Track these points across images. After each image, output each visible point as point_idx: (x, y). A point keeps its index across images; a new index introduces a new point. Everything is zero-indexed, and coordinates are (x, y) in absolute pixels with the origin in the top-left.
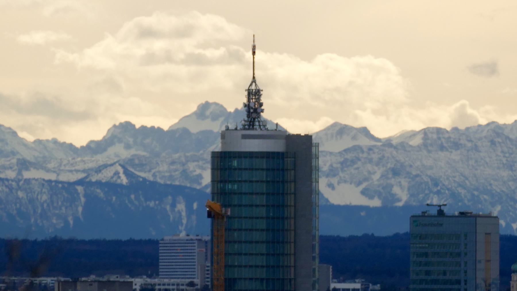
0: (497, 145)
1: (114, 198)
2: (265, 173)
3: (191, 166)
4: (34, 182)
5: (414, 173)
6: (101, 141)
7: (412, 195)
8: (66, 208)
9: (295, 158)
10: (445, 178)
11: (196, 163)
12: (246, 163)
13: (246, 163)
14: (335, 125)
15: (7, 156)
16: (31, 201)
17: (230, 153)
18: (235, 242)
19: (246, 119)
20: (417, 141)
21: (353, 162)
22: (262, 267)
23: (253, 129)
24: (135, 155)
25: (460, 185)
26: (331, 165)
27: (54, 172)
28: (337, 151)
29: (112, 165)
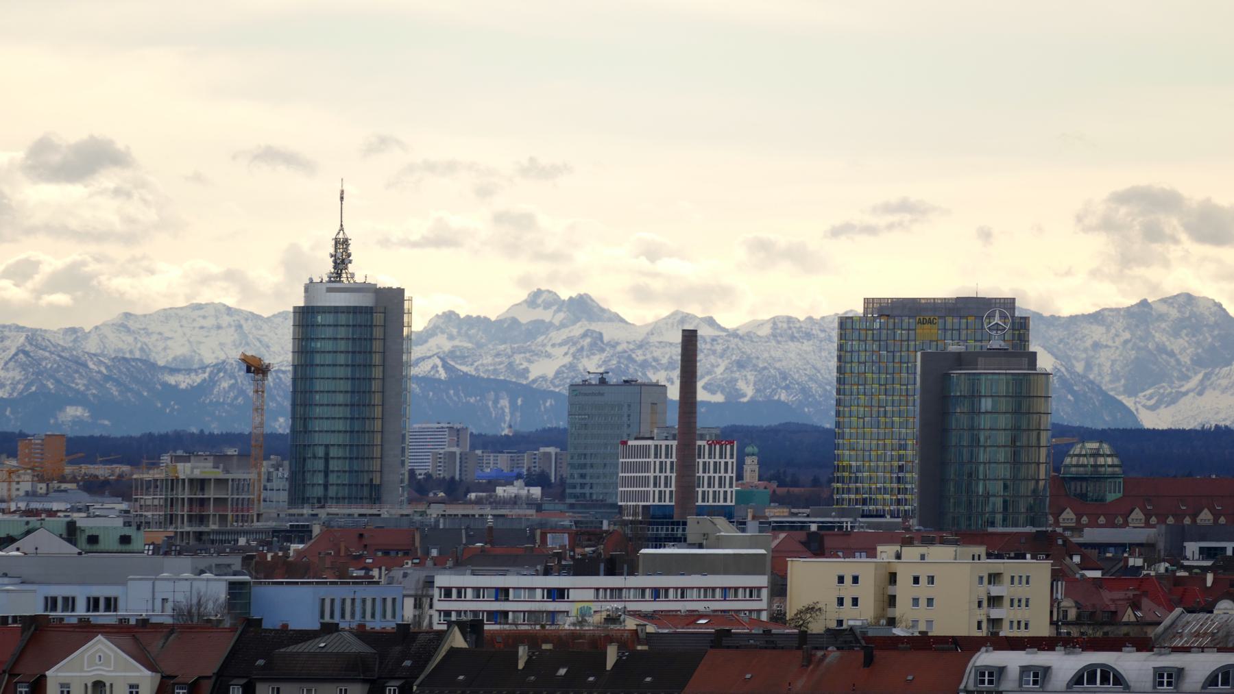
1: (431, 394)
3: (518, 358)
5: (761, 366)
6: (422, 332)
7: (758, 391)
9: (385, 313)
10: (795, 370)
11: (523, 355)
12: (330, 319)
13: (330, 319)
17: (313, 307)
19: (333, 270)
20: (765, 331)
23: (340, 281)
24: (457, 346)
25: (811, 379)
26: (671, 357)
29: (429, 357)
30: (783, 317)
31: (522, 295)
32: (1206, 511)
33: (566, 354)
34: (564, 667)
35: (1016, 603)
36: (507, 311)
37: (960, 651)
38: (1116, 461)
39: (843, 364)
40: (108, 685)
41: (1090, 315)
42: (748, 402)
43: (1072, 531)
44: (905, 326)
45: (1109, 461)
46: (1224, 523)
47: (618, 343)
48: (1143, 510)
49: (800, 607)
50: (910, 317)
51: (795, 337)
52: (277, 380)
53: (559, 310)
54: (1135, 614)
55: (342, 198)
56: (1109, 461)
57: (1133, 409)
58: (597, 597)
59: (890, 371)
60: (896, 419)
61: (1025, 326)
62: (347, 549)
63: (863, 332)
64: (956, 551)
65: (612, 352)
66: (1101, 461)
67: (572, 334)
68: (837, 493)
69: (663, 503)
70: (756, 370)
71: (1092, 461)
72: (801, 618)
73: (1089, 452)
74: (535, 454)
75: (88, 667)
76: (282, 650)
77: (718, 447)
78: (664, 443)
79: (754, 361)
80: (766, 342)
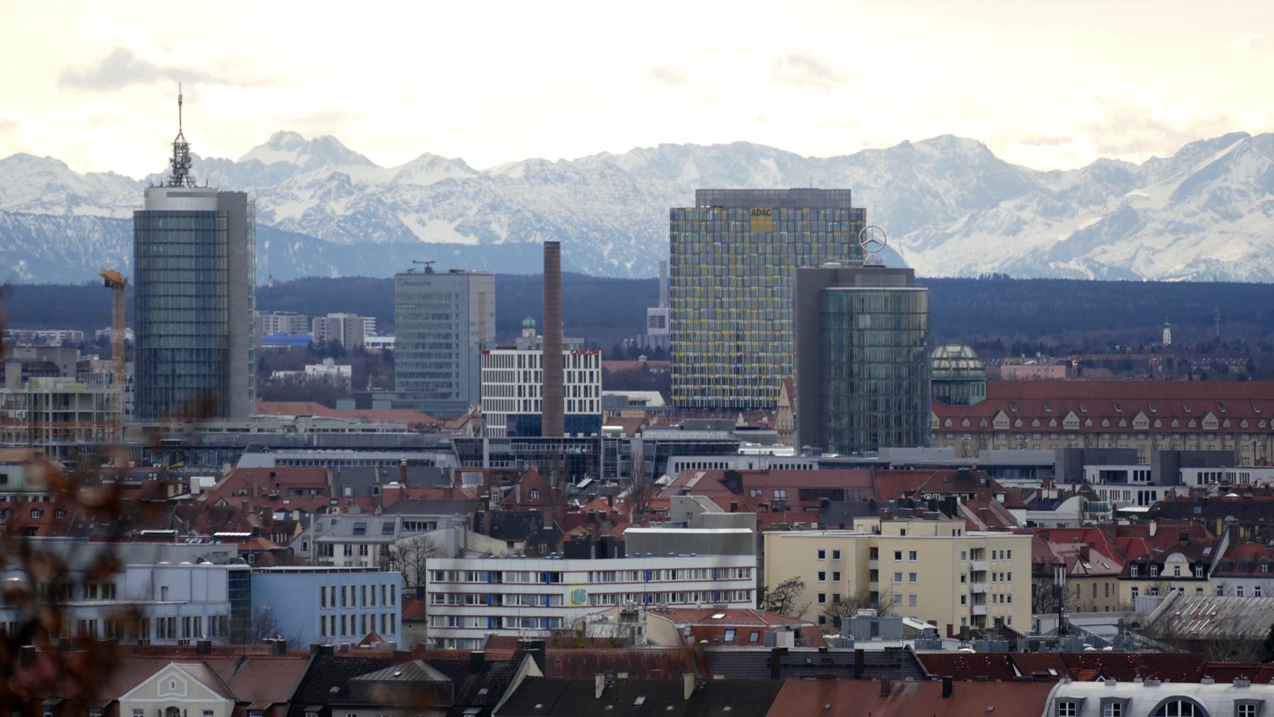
0: (609, 178)
2: (193, 233)
4: (85, 219)
5: (515, 208)
6: (162, 174)
7: (513, 233)
8: (122, 247)
11: (268, 198)
12: (172, 223)
13: (172, 223)
14: (425, 156)
15: (57, 191)
16: (82, 240)
17: (154, 212)
18: (161, 309)
19: (172, 175)
20: (518, 173)
21: (446, 197)
22: (192, 336)
23: (180, 186)
25: (567, 221)
26: (421, 200)
27: (108, 208)
28: (428, 184)
30: (536, 160)
31: (265, 138)
32: (1072, 413)
33: (313, 197)
34: (642, 695)
35: (998, 577)
36: (250, 153)
37: (1018, 674)
38: (978, 364)
39: (676, 255)
40: (182, 711)
41: (851, 157)
42: (503, 245)
44: (739, 217)
45: (972, 364)
47: (366, 186)
48: (1008, 413)
49: (782, 582)
50: (743, 208)
51: (549, 180)
52: (16, 223)
53: (303, 152)
54: (1084, 567)
55: (180, 103)
56: (972, 364)
57: (898, 251)
58: (591, 580)
59: (725, 261)
60: (733, 310)
61: (861, 218)
62: (259, 488)
63: (696, 223)
64: (936, 526)
65: (360, 195)
66: (963, 364)
67: (318, 177)
68: (675, 384)
69: (528, 413)
70: (510, 213)
71: (954, 364)
72: (783, 593)
74: (323, 320)
75: (161, 693)
76: (357, 678)
77: (582, 357)
78: (527, 353)
79: (508, 204)
80: (520, 185)
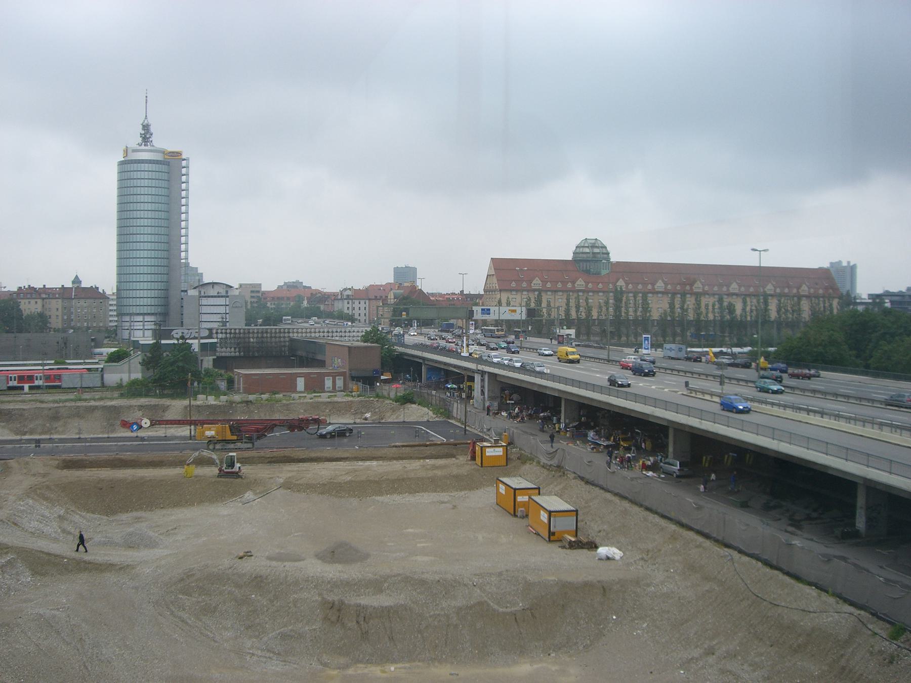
43: (517, 292)
46: (688, 289)
73: (590, 245)
